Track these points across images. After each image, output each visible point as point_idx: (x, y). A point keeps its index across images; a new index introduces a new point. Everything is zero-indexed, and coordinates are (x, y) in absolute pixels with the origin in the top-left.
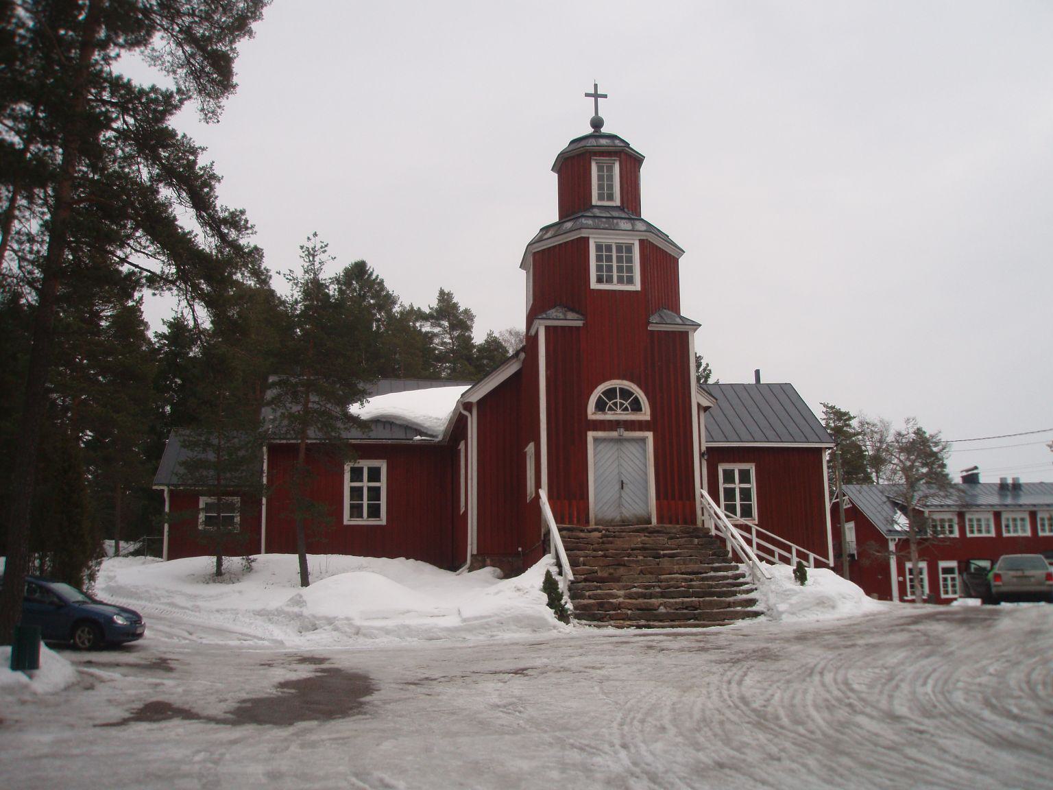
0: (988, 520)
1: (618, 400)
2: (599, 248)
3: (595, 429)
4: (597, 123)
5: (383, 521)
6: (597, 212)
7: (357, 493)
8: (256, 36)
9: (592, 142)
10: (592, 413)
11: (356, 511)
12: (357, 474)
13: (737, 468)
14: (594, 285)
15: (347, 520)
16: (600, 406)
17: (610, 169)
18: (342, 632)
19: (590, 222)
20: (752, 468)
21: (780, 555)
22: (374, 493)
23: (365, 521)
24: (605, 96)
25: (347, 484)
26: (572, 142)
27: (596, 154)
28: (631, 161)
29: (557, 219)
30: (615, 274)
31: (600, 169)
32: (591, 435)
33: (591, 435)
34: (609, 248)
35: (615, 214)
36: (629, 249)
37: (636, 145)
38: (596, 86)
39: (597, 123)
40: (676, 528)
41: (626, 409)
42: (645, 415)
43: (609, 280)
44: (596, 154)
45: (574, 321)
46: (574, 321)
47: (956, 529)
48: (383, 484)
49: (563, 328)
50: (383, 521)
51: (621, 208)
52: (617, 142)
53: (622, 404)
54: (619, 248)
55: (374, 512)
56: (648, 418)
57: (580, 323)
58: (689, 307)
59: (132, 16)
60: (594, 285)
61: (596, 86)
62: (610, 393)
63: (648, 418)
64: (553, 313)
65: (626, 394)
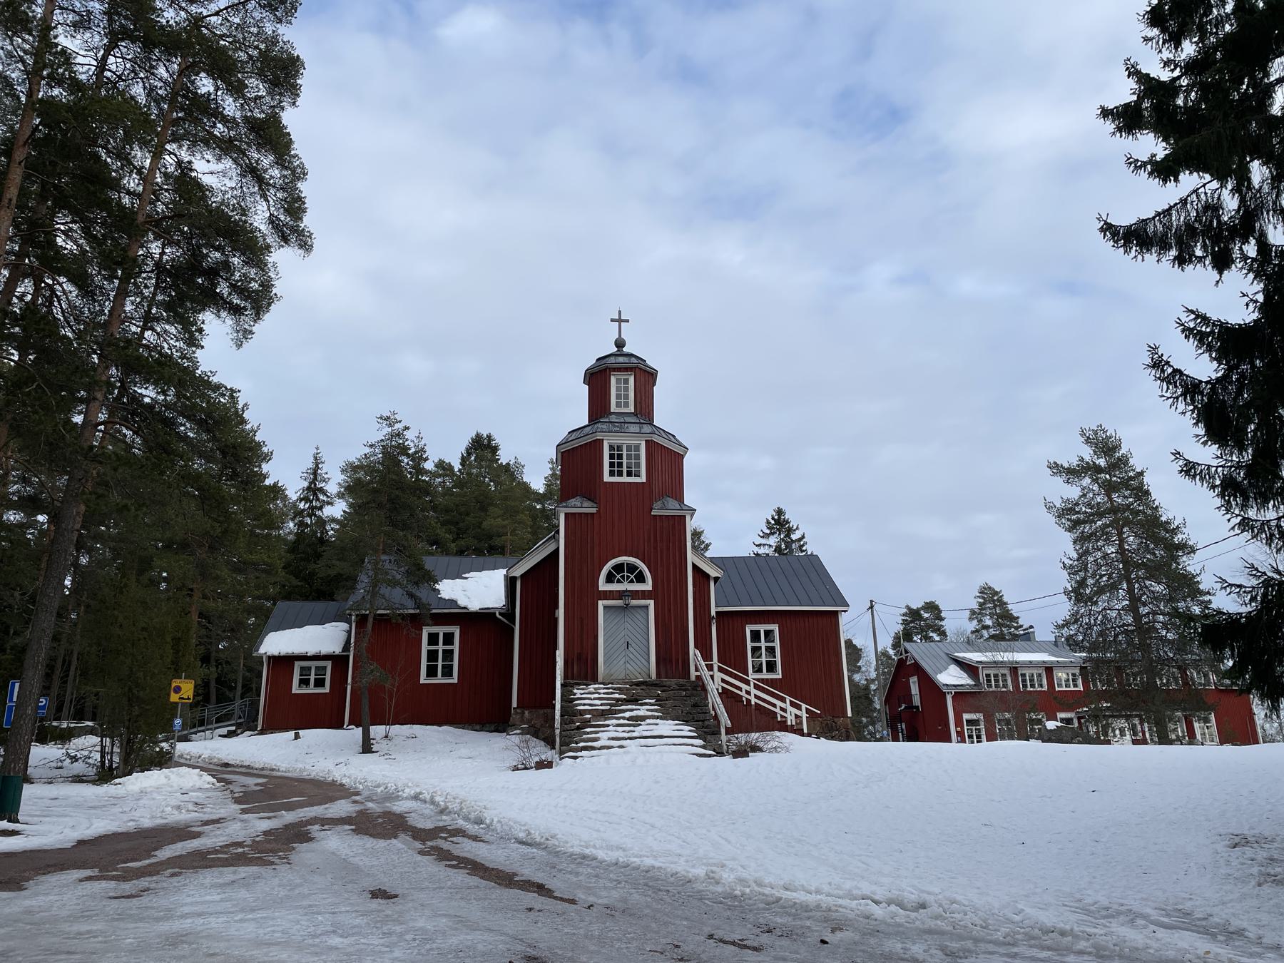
0: (1039, 675)
1: (625, 574)
2: (611, 448)
3: (606, 598)
4: (620, 344)
5: (455, 680)
6: (613, 418)
7: (432, 656)
8: (317, 243)
9: (612, 360)
10: (603, 586)
11: (432, 672)
12: (756, 637)
13: (762, 628)
14: (607, 478)
15: (423, 679)
16: (610, 579)
17: (626, 381)
18: (1119, 913)
19: (604, 426)
20: (775, 628)
21: (790, 701)
22: (448, 655)
23: (439, 680)
24: (628, 321)
25: (425, 648)
26: (598, 360)
27: (615, 370)
28: (646, 377)
29: (587, 423)
30: (625, 469)
31: (618, 381)
32: (601, 603)
33: (601, 603)
34: (620, 448)
35: (628, 419)
36: (637, 448)
37: (651, 362)
38: (620, 312)
39: (620, 344)
40: (672, 682)
41: (632, 581)
42: (648, 586)
43: (620, 474)
44: (615, 370)
45: (589, 508)
46: (589, 508)
47: (1045, 682)
48: (456, 648)
49: (580, 514)
50: (455, 680)
51: (635, 414)
52: (633, 360)
53: (628, 577)
54: (629, 449)
55: (448, 671)
56: (650, 588)
57: (594, 510)
58: (691, 497)
59: (13, 327)
60: (607, 478)
61: (620, 312)
62: (619, 568)
63: (650, 588)
64: (573, 502)
65: (632, 568)
